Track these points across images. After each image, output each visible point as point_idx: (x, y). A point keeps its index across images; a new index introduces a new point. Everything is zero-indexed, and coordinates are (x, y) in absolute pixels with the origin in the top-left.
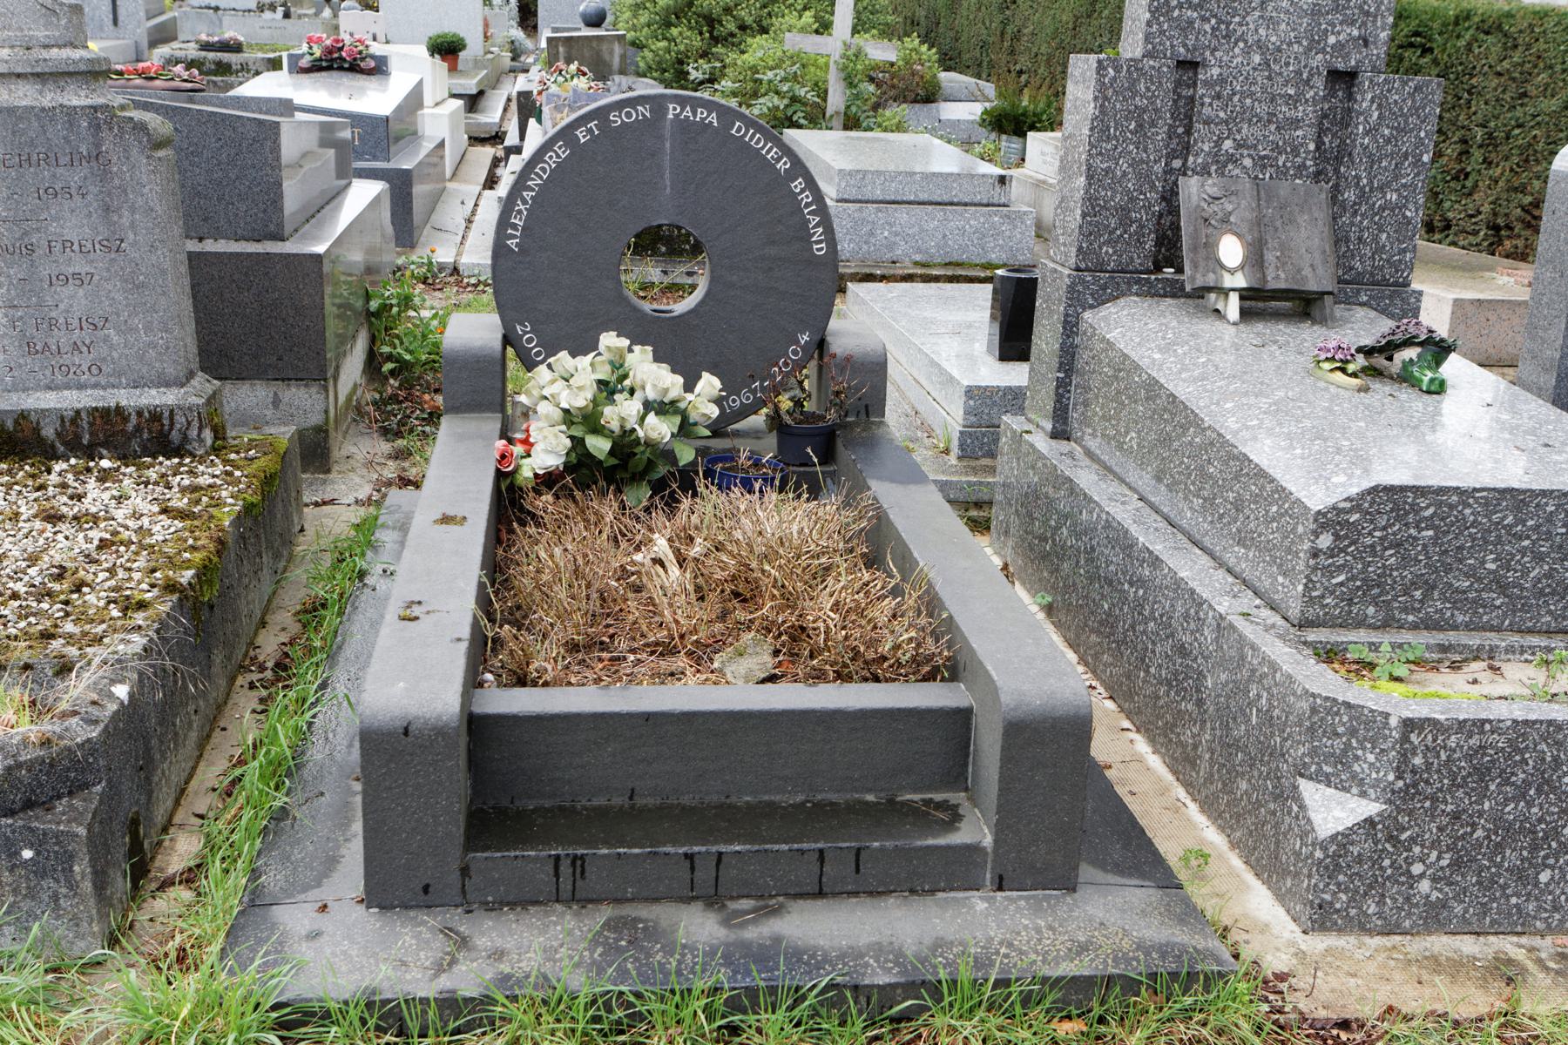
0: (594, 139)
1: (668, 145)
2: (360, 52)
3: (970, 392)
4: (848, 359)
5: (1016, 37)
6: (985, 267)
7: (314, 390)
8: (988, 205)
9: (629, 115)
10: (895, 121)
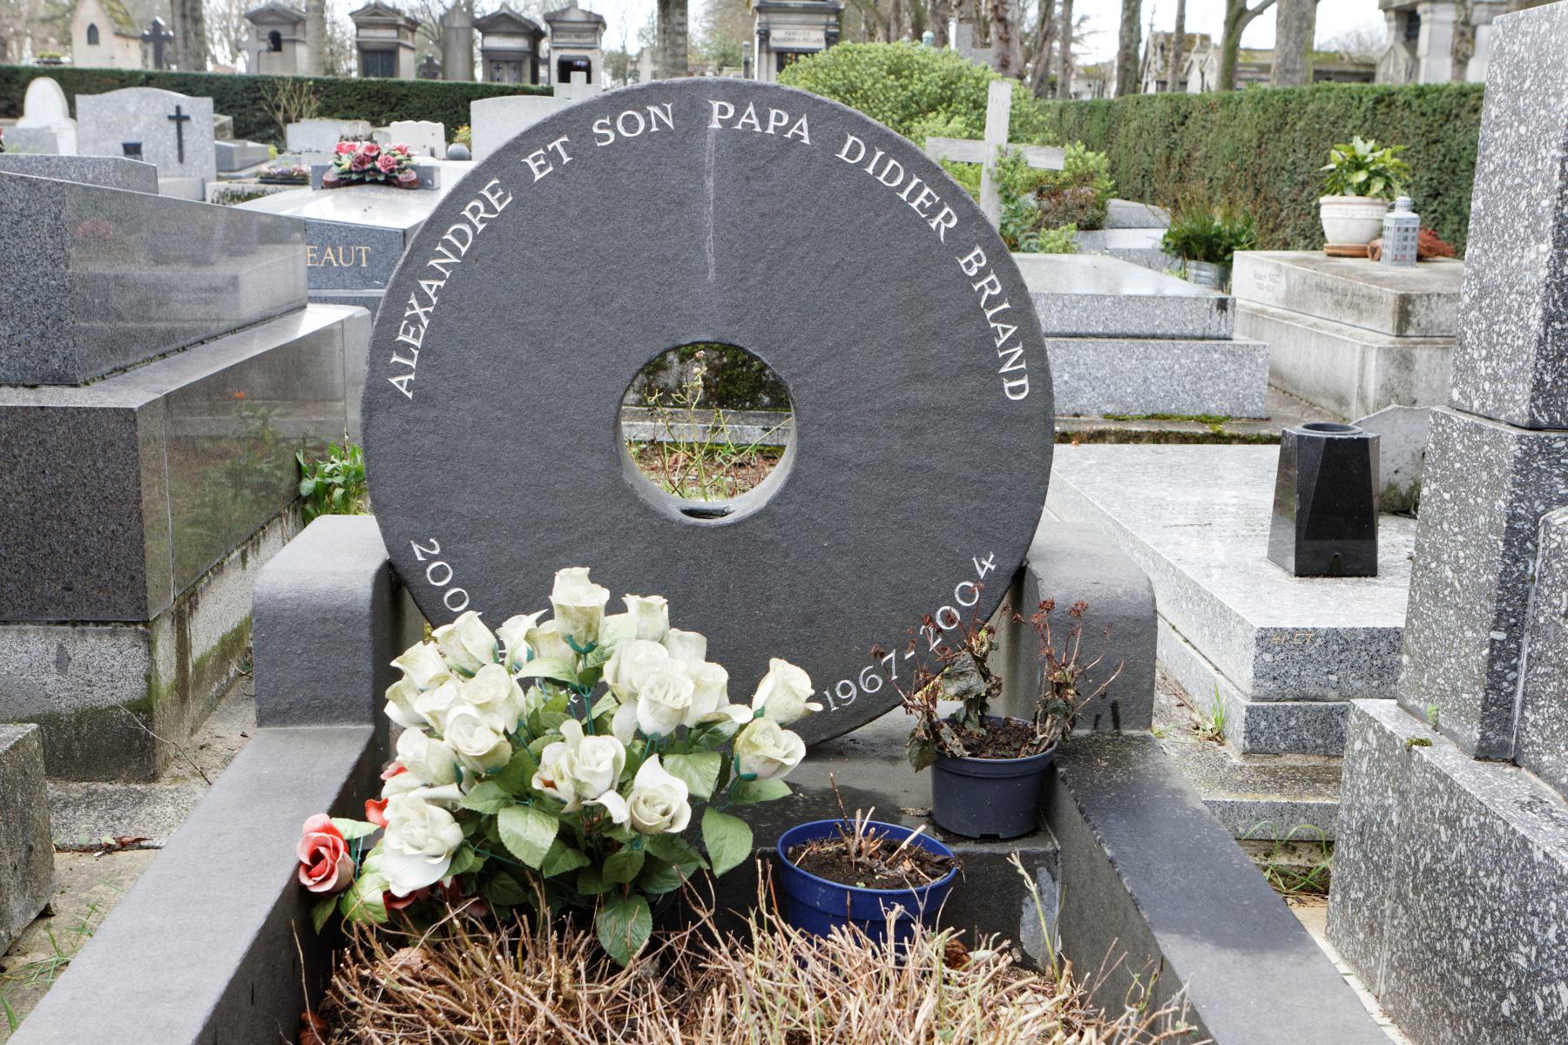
0: (561, 173)
1: (710, 183)
2: (399, 162)
3: (1265, 640)
4: (1078, 611)
5: (1186, 162)
6: (1203, 420)
7: (126, 640)
8: (1203, 338)
9: (630, 123)
10: (1060, 243)
